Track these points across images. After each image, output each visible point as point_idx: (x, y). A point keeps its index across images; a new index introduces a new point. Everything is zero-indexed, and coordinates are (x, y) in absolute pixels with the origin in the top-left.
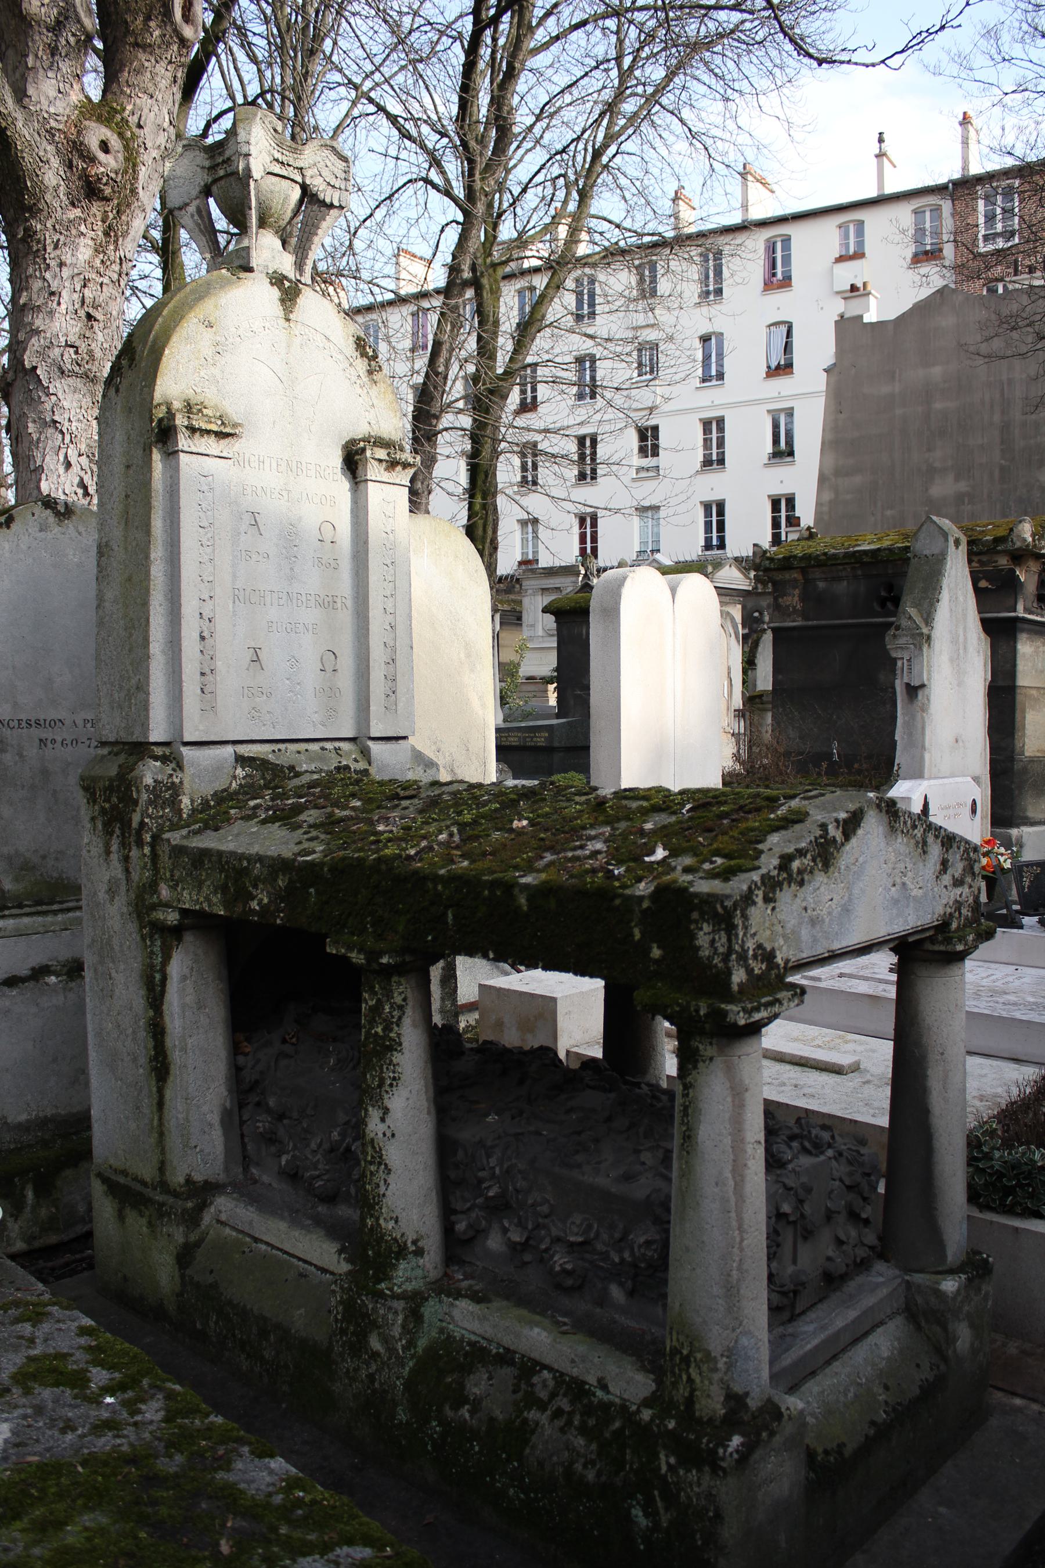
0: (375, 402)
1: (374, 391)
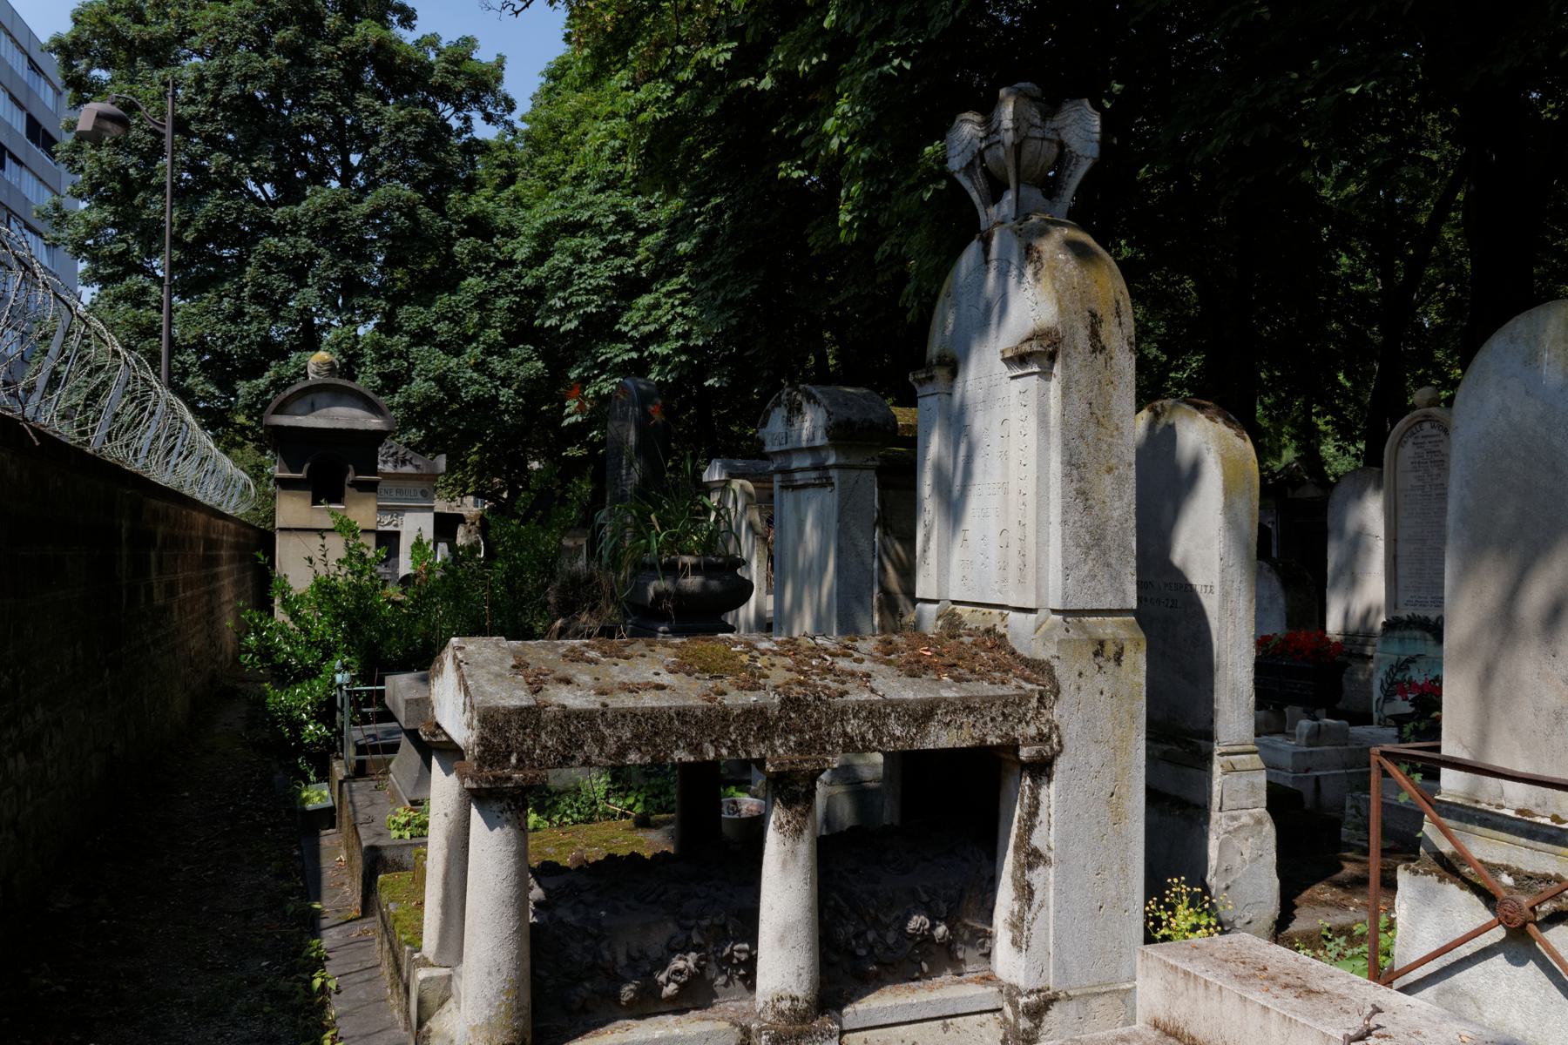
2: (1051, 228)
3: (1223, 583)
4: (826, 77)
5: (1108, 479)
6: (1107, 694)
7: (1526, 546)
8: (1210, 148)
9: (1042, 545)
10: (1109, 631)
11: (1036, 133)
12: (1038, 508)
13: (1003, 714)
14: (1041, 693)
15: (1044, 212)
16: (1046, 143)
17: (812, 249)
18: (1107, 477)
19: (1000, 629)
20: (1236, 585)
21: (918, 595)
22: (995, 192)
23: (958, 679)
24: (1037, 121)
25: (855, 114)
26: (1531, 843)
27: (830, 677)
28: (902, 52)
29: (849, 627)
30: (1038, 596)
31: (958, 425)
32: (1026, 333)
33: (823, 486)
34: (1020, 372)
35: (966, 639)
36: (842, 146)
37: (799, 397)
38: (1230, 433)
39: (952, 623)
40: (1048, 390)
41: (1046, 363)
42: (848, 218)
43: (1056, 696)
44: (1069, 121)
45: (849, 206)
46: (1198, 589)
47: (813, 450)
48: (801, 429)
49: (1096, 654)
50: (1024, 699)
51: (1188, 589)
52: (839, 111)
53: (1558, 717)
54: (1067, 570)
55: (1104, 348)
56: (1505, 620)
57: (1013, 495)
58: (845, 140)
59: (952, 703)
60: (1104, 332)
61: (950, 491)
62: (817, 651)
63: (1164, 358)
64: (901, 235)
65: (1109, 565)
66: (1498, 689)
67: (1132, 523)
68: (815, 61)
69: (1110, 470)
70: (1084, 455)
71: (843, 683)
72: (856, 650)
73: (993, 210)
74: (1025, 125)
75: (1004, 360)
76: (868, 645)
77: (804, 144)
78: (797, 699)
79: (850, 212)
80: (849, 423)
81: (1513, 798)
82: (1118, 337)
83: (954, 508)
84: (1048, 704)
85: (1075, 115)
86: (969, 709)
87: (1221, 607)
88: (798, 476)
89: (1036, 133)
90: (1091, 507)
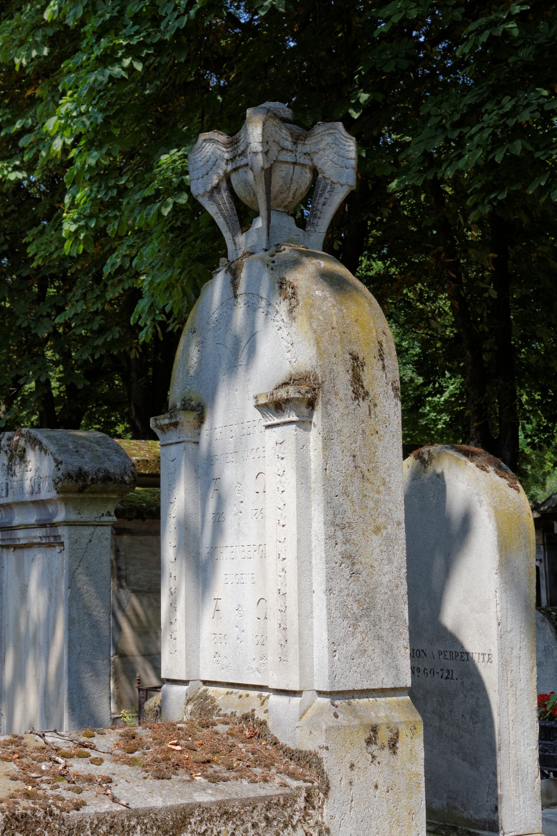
2: (305, 260)
3: (501, 650)
4: (47, 70)
5: (376, 540)
6: (382, 788)
8: (461, 164)
9: (305, 616)
10: (382, 714)
11: (287, 157)
12: (299, 575)
13: (267, 818)
14: (308, 790)
15: (297, 242)
16: (297, 168)
17: (32, 259)
18: (374, 537)
19: (260, 715)
20: (515, 652)
21: (163, 676)
22: (244, 216)
23: (214, 779)
24: (288, 144)
25: (81, 114)
27: (64, 784)
28: (130, 50)
29: (85, 718)
30: (302, 676)
31: (206, 473)
32: (282, 377)
33: (50, 545)
34: (276, 421)
35: (222, 728)
36: (65, 150)
37: (22, 443)
38: (503, 482)
39: (204, 708)
40: (308, 441)
41: (305, 410)
42: (73, 228)
43: (326, 794)
44: (321, 146)
45: (74, 214)
46: (476, 657)
47: (40, 504)
48: (22, 480)
49: (369, 742)
50: (288, 801)
51: (465, 657)
52: (62, 110)
54: (334, 646)
55: (367, 394)
57: (271, 559)
58: (69, 141)
59: (208, 809)
60: (366, 377)
61: (198, 554)
62: (48, 752)
63: (420, 380)
64: (131, 246)
65: (379, 638)
67: (404, 589)
68: (34, 53)
69: (377, 530)
70: (349, 514)
71: (79, 791)
72: (93, 748)
73: (241, 238)
74: (274, 149)
75: (258, 406)
76: (107, 741)
77: (22, 143)
78: (24, 816)
79: (75, 221)
80: (81, 474)
82: (384, 379)
83: (202, 570)
84: (317, 803)
85: (329, 139)
86: (227, 815)
87: (502, 678)
88: (20, 534)
89: (288, 157)
90: (358, 573)
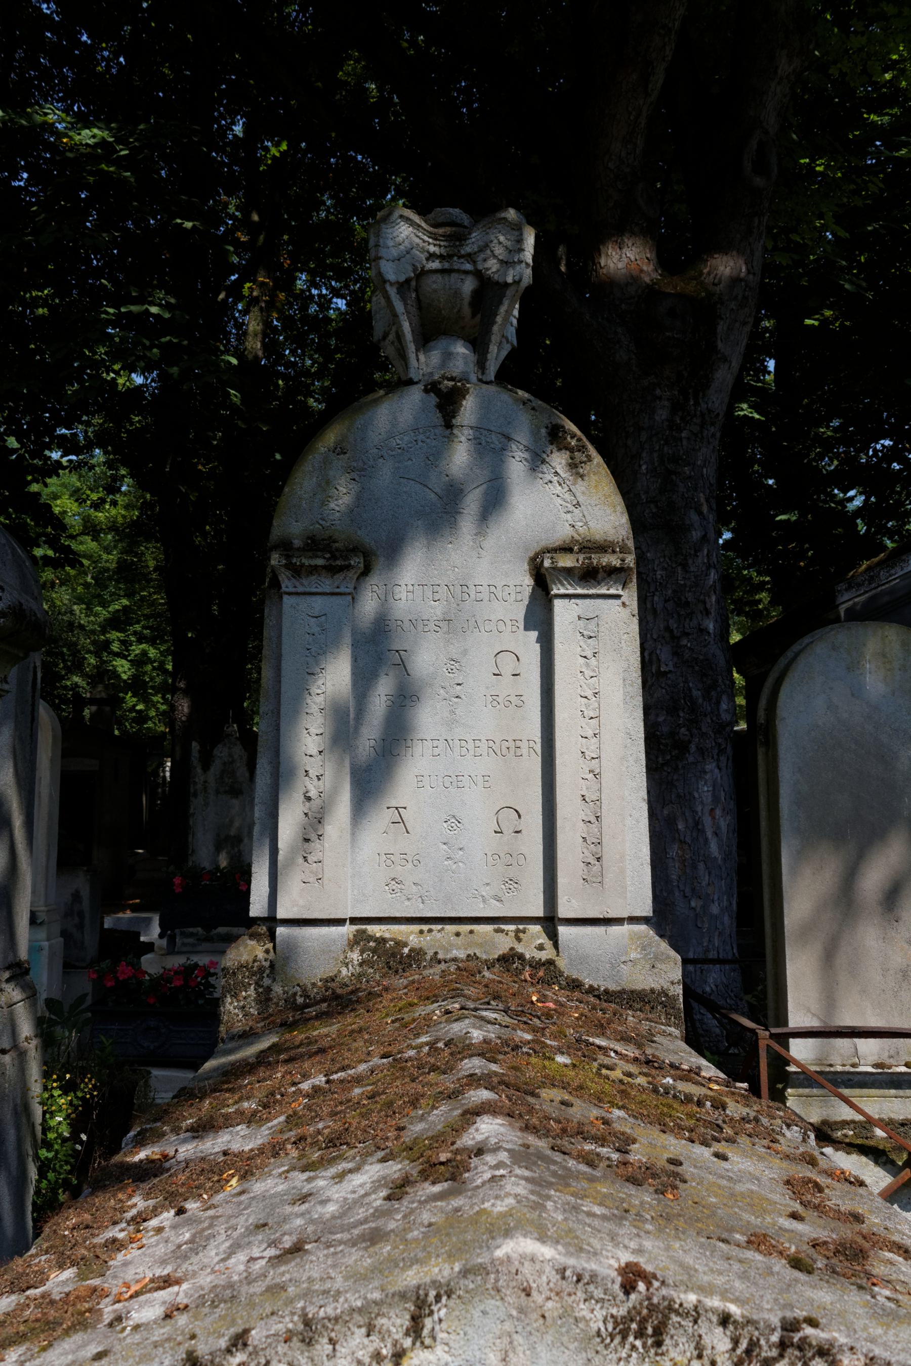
0: (581, 499)
1: (580, 487)
7: (856, 834)
26: (901, 1092)
53: (904, 974)
56: (845, 899)
66: (842, 959)
81: (869, 1053)
